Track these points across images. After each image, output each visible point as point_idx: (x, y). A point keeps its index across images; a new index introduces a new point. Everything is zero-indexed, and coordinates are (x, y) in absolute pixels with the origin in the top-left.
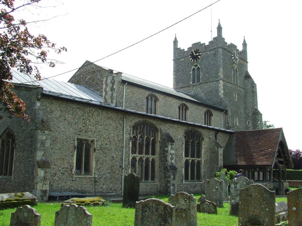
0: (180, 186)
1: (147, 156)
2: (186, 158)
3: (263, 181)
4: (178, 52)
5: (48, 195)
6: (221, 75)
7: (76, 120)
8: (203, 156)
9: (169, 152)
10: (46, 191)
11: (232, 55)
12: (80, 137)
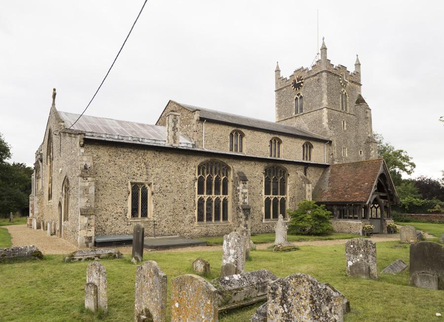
0: (259, 225)
1: (217, 196)
2: (267, 196)
3: (364, 218)
4: (279, 79)
5: (93, 241)
6: (325, 102)
7: (129, 164)
8: (288, 193)
9: (241, 191)
10: (91, 237)
11: (340, 79)
12: (134, 181)
